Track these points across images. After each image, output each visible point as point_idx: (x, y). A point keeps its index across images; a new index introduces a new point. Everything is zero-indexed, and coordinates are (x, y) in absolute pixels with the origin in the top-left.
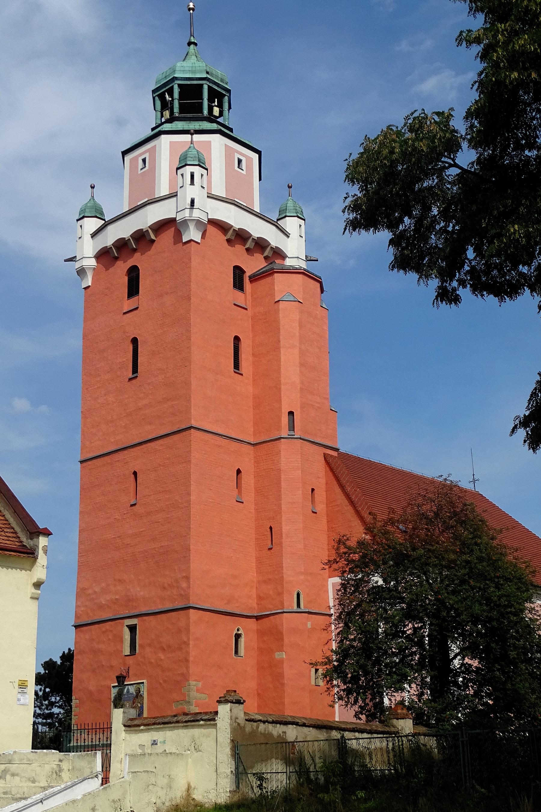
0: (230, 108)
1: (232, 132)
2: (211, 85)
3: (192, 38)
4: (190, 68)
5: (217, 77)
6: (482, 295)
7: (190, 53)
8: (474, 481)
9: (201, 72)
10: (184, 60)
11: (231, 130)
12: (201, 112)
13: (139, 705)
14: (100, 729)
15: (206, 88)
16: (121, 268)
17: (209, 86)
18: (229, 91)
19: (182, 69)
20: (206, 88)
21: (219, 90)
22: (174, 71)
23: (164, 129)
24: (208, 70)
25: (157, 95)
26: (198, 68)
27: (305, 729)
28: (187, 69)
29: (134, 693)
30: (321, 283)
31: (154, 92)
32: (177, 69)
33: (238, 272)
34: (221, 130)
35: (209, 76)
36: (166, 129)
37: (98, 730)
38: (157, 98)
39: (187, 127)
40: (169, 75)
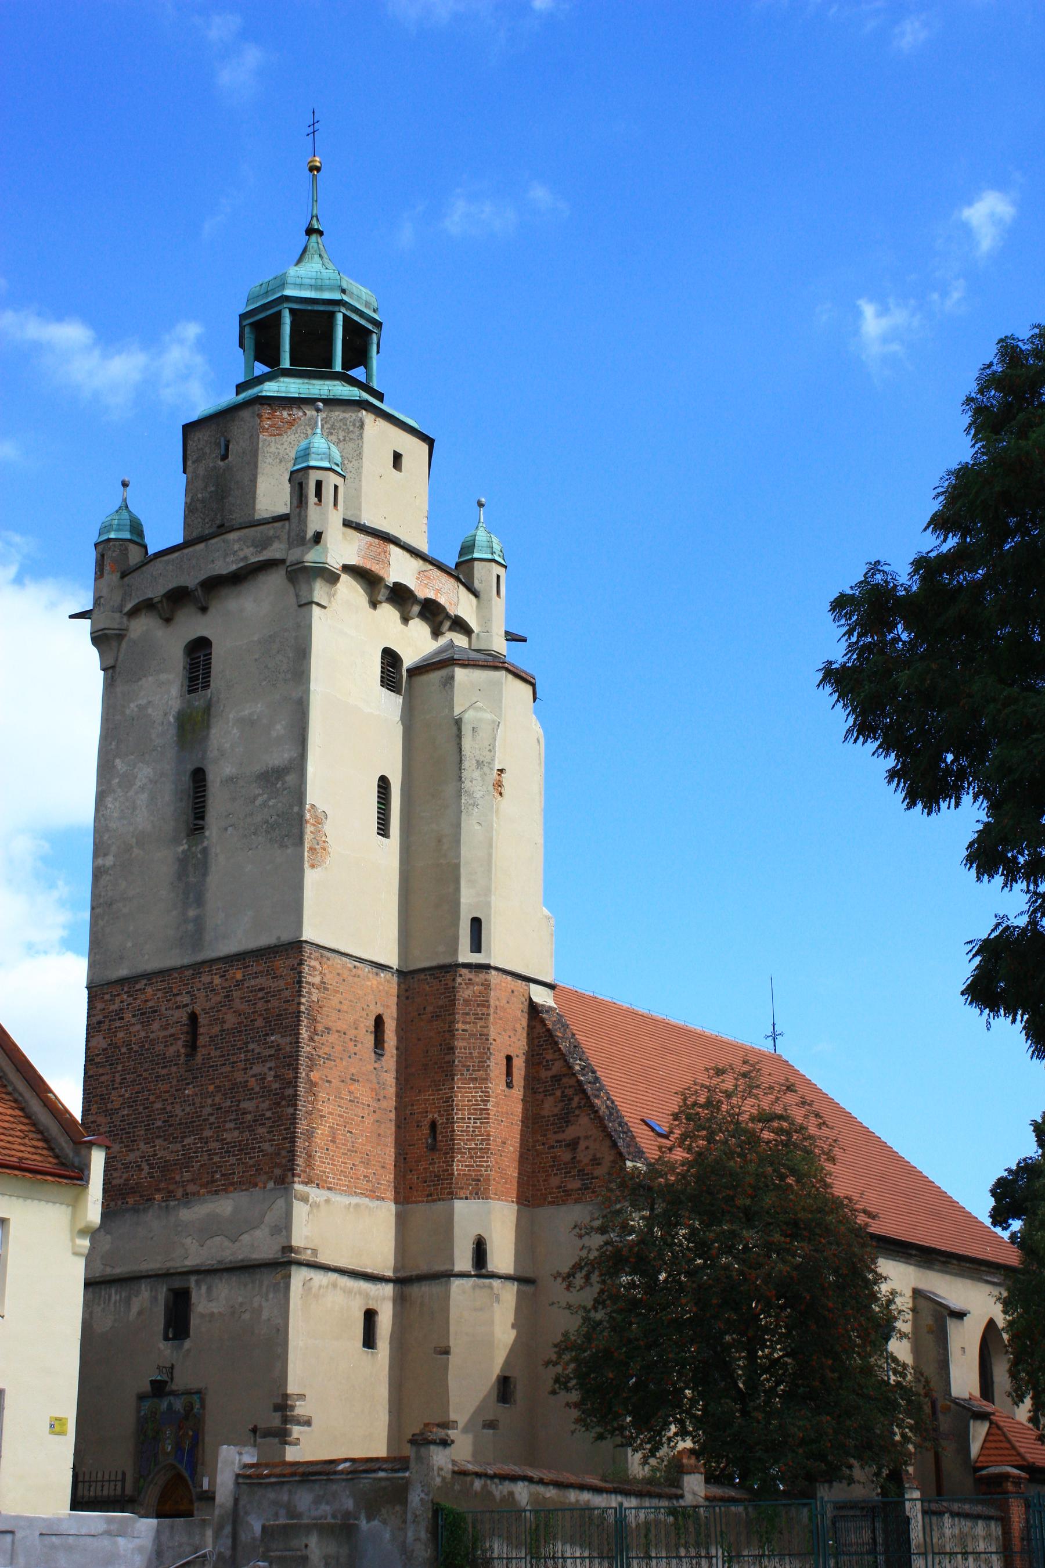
0: (378, 352)
1: (382, 401)
2: (348, 313)
3: (314, 221)
4: (308, 278)
5: (359, 298)
6: (1030, 1411)
7: (311, 250)
8: (774, 1036)
9: (331, 289)
10: (299, 261)
11: (380, 396)
12: (329, 362)
13: (191, 1433)
14: (109, 1481)
15: (340, 318)
16: (170, 642)
17: (344, 315)
18: (378, 325)
19: (298, 281)
20: (340, 318)
21: (363, 322)
22: (283, 285)
23: (264, 394)
24: (345, 286)
25: (251, 324)
26: (327, 282)
27: (541, 1489)
28: (307, 281)
29: (182, 1411)
30: (533, 685)
31: (243, 317)
32: (290, 280)
33: (390, 658)
34: (367, 402)
35: (345, 298)
36: (268, 394)
37: (106, 1484)
38: (247, 330)
39: (307, 391)
40: (274, 291)
